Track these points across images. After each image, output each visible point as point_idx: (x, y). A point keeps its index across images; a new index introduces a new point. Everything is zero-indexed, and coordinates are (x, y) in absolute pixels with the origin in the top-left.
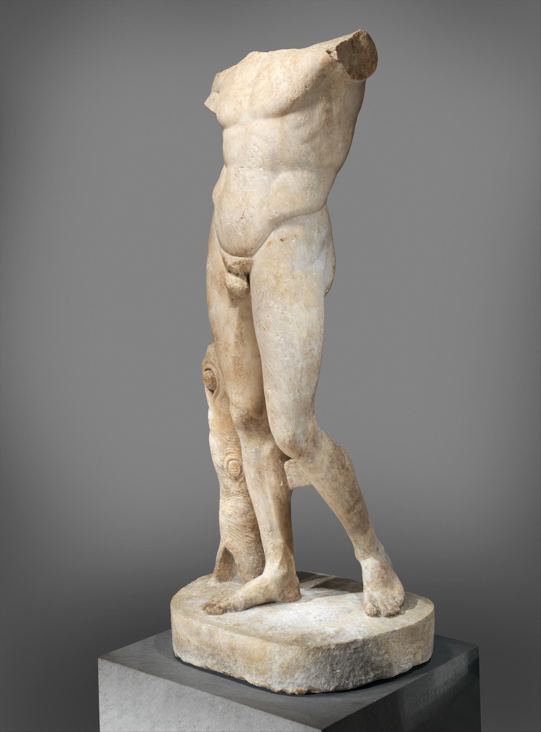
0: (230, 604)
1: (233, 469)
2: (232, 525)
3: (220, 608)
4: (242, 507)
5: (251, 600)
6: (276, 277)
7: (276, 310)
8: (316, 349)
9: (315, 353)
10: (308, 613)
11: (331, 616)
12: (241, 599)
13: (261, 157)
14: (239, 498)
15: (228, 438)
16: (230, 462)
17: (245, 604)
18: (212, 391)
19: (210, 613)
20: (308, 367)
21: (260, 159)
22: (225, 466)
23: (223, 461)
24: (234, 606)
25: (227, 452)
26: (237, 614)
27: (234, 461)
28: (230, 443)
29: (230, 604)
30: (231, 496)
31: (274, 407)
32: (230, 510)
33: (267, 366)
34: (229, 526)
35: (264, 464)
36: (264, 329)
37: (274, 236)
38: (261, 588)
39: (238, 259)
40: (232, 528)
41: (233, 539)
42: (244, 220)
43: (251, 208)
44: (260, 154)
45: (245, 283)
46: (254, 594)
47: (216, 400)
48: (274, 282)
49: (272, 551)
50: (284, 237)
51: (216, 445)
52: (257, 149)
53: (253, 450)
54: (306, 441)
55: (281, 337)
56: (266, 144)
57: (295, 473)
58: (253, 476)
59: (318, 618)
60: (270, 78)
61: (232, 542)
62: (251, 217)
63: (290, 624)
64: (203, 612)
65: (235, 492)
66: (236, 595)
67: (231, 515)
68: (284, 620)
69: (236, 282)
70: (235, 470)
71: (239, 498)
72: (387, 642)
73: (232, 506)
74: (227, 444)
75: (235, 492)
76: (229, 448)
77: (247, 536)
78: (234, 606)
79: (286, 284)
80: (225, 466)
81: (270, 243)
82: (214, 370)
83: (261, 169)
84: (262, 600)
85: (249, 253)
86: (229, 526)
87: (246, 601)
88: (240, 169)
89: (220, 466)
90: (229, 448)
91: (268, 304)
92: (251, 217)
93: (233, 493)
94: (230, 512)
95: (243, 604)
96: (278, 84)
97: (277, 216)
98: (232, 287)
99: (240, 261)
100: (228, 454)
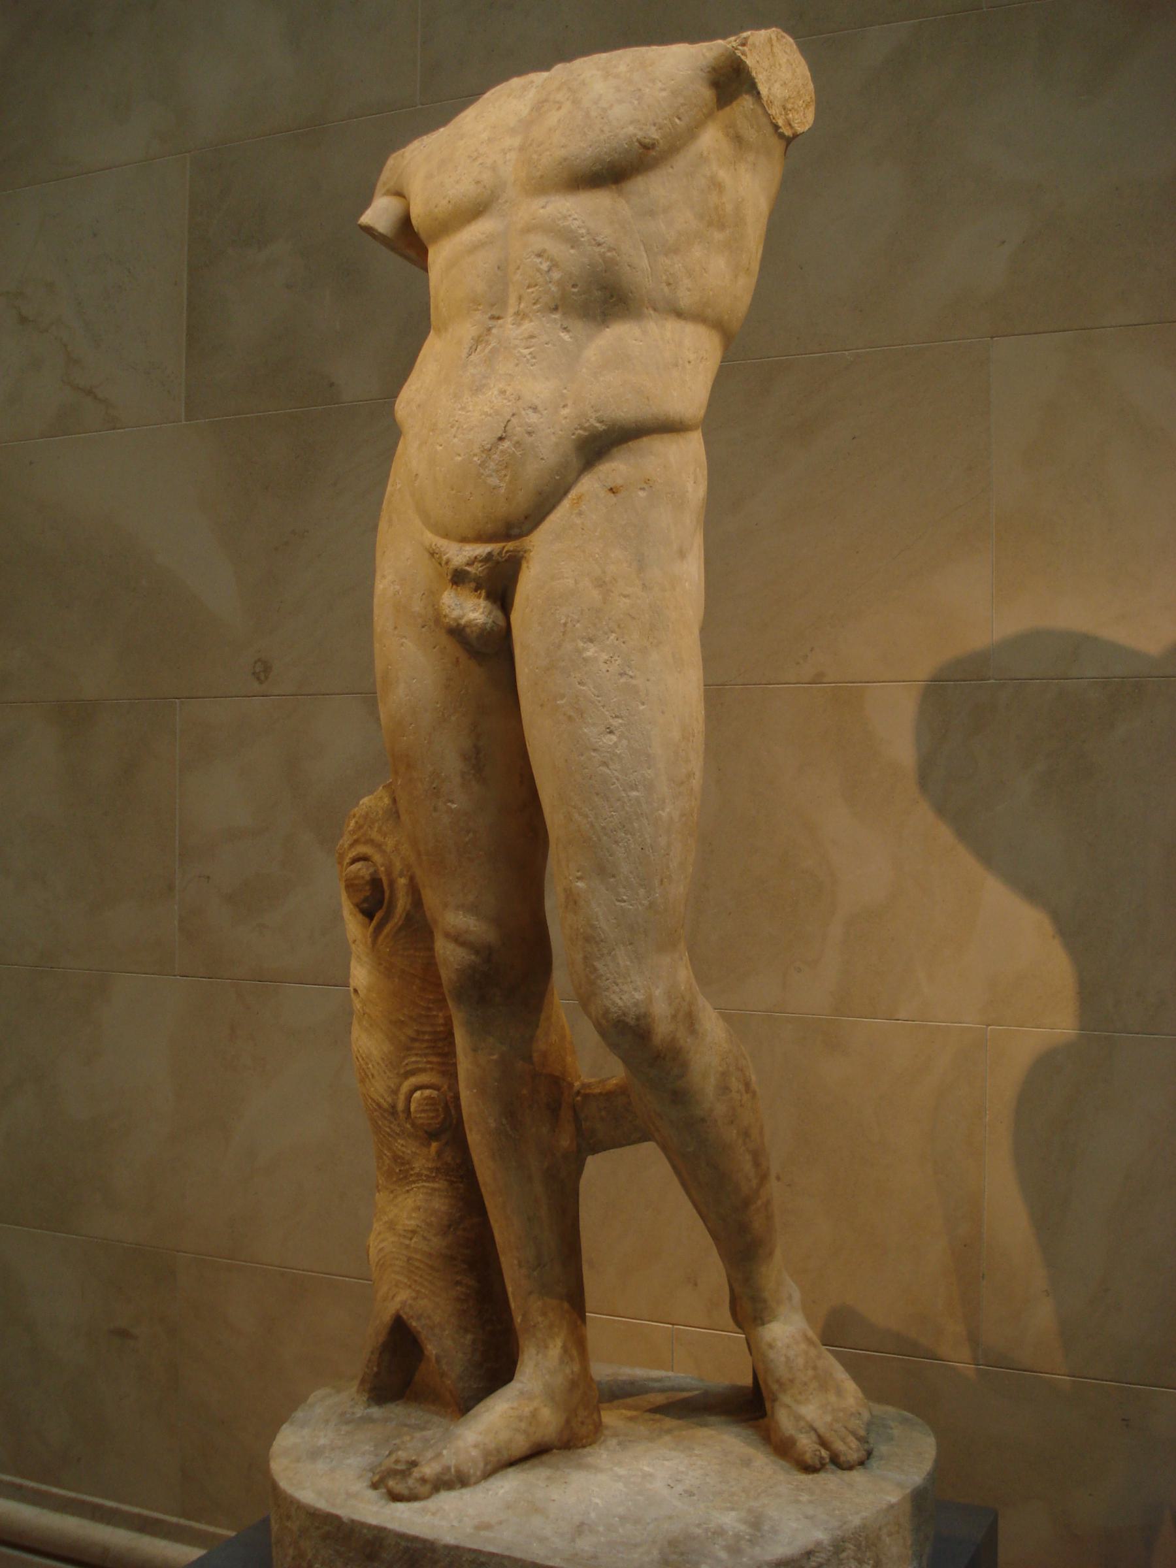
0: (449, 1468)
1: (423, 1111)
2: (418, 1256)
3: (423, 1480)
4: (444, 1208)
5: (498, 1451)
6: (600, 583)
7: (604, 667)
8: (698, 775)
9: (696, 783)
10: (647, 1476)
11: (708, 1479)
12: (474, 1453)
13: (559, 283)
14: (436, 1185)
15: (411, 1033)
16: (417, 1094)
17: (486, 1464)
18: (369, 914)
19: (396, 1497)
20: (684, 819)
21: (554, 288)
22: (401, 1106)
23: (395, 1092)
24: (458, 1471)
25: (408, 1068)
26: (466, 1493)
27: (427, 1092)
28: (417, 1045)
29: (449, 1468)
30: (414, 1182)
31: (593, 927)
32: (410, 1218)
33: (576, 816)
34: (409, 1259)
35: (525, 1092)
36: (570, 718)
37: (589, 484)
38: (520, 1418)
39: (482, 550)
40: (417, 1264)
41: (418, 1292)
42: (506, 444)
43: (530, 412)
44: (556, 275)
45: (498, 614)
46: (504, 1435)
47: (381, 938)
48: (596, 594)
49: (540, 1319)
50: (620, 482)
51: (375, 1052)
52: (545, 266)
53: (495, 1057)
54: (674, 1017)
55: (620, 738)
56: (572, 251)
57: (603, 1113)
58: (493, 1125)
59: (679, 1488)
60: (576, 102)
61: (415, 1299)
62: (530, 433)
63: (621, 1510)
64: (372, 1494)
65: (425, 1172)
66: (460, 1444)
67: (414, 1232)
68: (598, 1501)
69: (474, 611)
70: (431, 1114)
71: (436, 1185)
72: (879, 1538)
73: (419, 1208)
74: (409, 1049)
75: (425, 1172)
76: (414, 1059)
77: (458, 1283)
78: (458, 1471)
79: (627, 601)
80: (401, 1106)
81: (580, 498)
82: (377, 858)
83: (556, 316)
84: (521, 1445)
85: (516, 531)
86: (409, 1259)
87: (487, 1454)
88: (491, 323)
89: (385, 1105)
90: (414, 1059)
91: (579, 652)
92: (530, 433)
93: (419, 1175)
94: (412, 1224)
95: (481, 1465)
96: (604, 110)
97: (601, 427)
98: (463, 622)
99: (490, 554)
100: (412, 1073)
